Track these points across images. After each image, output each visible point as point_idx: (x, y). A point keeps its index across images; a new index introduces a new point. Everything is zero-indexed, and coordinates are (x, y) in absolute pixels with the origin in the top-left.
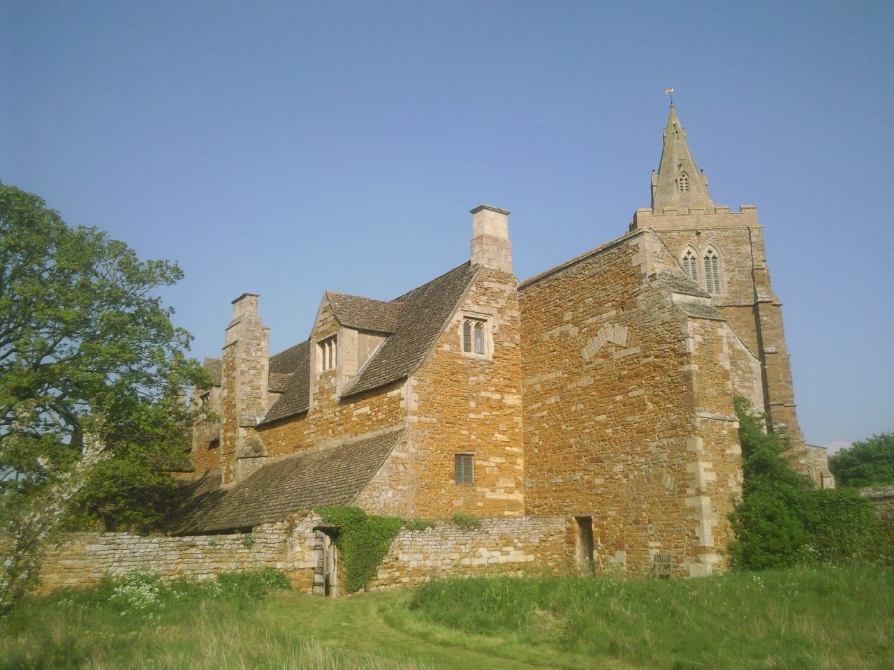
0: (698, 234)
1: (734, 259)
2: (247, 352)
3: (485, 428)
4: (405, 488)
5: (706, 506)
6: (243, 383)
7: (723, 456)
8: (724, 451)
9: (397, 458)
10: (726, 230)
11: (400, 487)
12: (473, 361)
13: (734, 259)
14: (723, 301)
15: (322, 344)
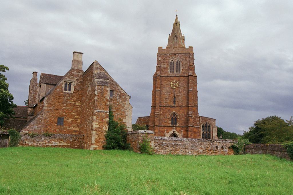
0: (175, 55)
1: (185, 62)
3: (68, 111)
4: (41, 126)
5: (94, 134)
6: (31, 96)
8: (103, 120)
9: (39, 118)
10: (183, 54)
11: (40, 125)
12: (67, 93)
13: (185, 62)
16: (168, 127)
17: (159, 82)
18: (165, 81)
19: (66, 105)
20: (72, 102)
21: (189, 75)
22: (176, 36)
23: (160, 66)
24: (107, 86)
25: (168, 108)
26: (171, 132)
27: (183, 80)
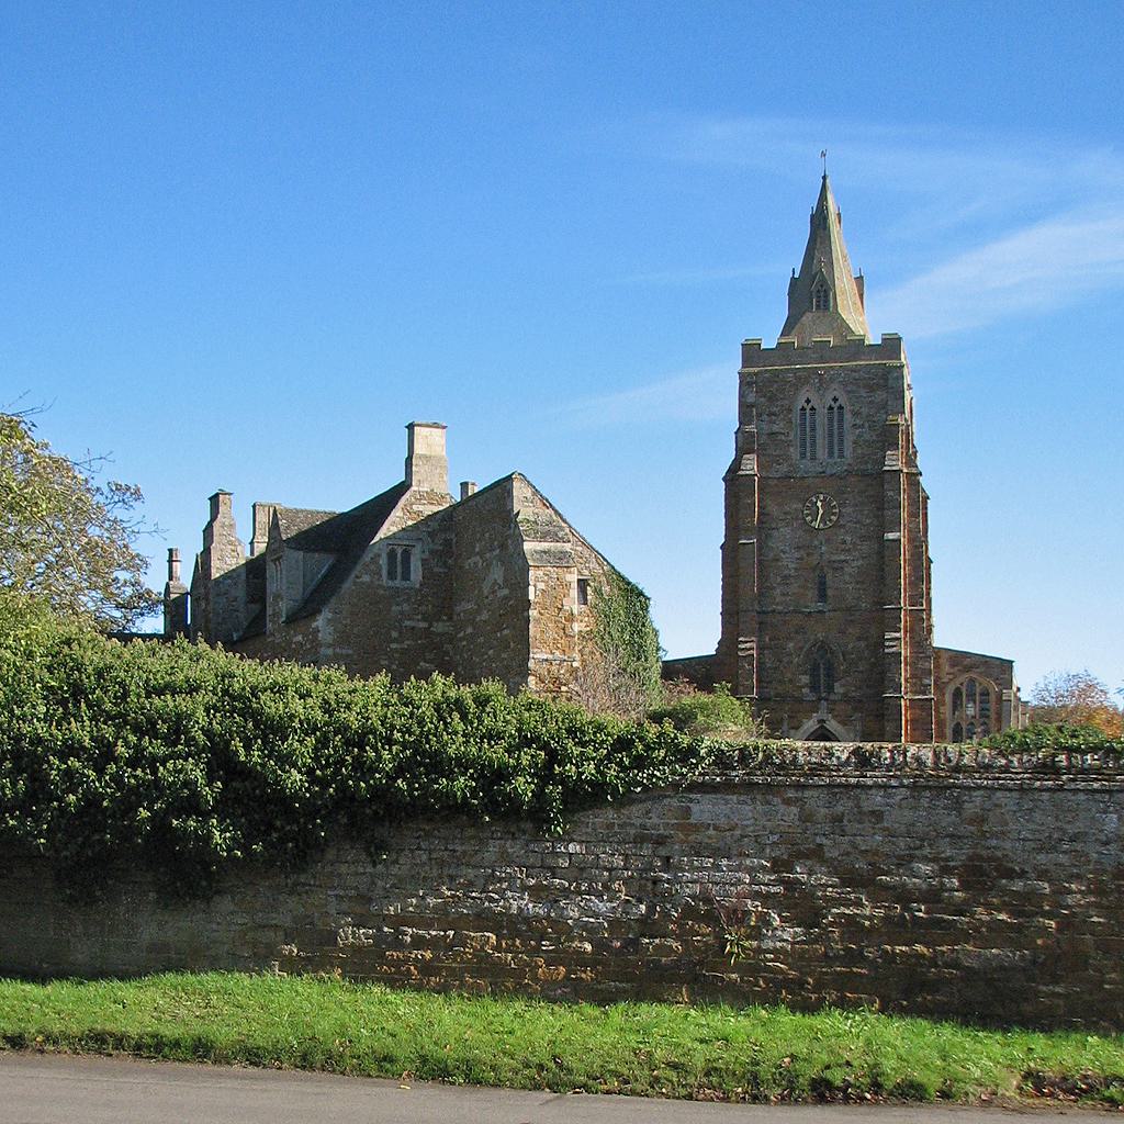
1: (865, 410)
13: (865, 410)
15: (274, 561)
20: (418, 620)
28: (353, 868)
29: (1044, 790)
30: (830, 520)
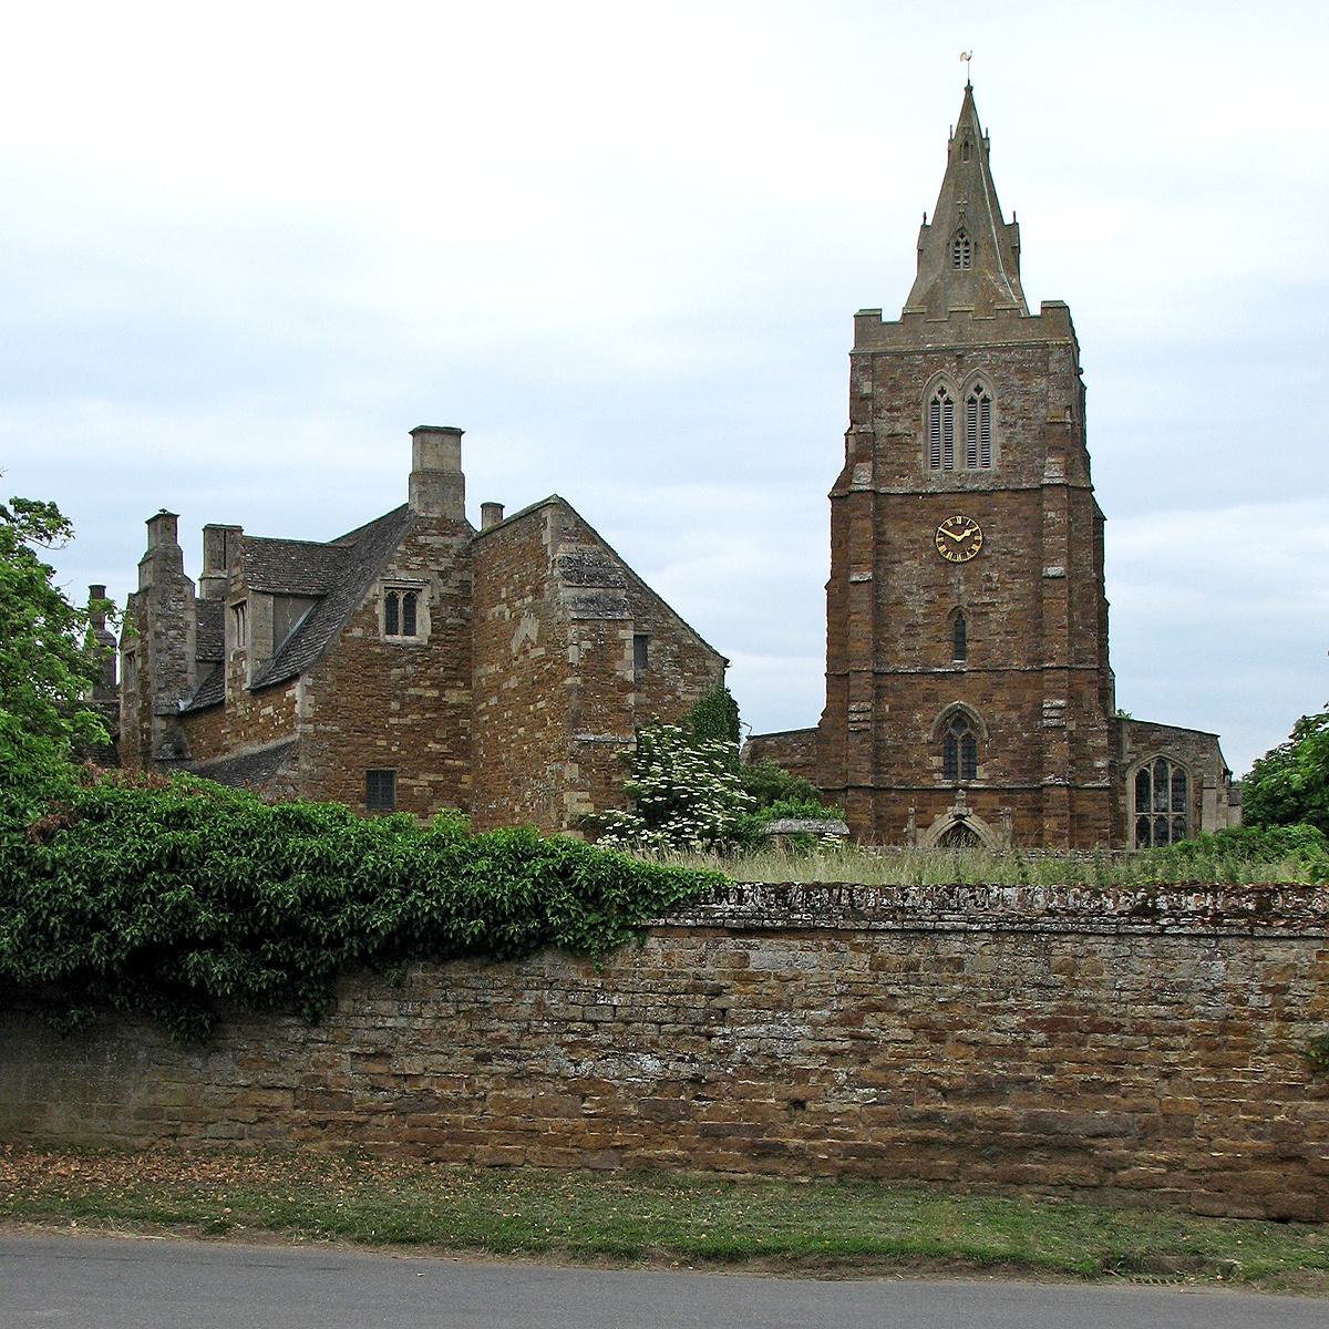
2: (163, 603)
7: (607, 784)
13: (1017, 404)
14: (991, 480)
15: (235, 608)
16: (927, 796)
17: (865, 530)
18: (904, 519)
19: (403, 706)
21: (1046, 481)
22: (969, 226)
23: (866, 427)
24: (622, 620)
25: (925, 683)
26: (944, 822)
27: (1012, 514)
28: (371, 1022)
29: (1142, 935)
30: (971, 551)
